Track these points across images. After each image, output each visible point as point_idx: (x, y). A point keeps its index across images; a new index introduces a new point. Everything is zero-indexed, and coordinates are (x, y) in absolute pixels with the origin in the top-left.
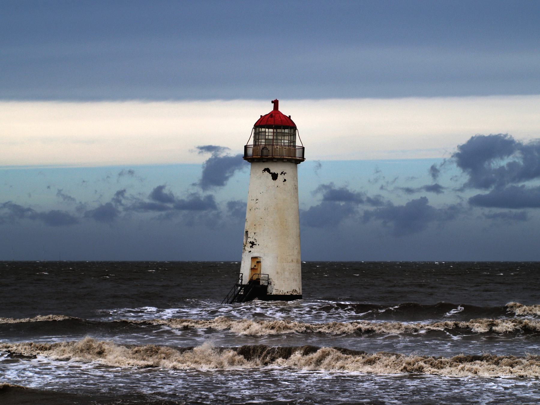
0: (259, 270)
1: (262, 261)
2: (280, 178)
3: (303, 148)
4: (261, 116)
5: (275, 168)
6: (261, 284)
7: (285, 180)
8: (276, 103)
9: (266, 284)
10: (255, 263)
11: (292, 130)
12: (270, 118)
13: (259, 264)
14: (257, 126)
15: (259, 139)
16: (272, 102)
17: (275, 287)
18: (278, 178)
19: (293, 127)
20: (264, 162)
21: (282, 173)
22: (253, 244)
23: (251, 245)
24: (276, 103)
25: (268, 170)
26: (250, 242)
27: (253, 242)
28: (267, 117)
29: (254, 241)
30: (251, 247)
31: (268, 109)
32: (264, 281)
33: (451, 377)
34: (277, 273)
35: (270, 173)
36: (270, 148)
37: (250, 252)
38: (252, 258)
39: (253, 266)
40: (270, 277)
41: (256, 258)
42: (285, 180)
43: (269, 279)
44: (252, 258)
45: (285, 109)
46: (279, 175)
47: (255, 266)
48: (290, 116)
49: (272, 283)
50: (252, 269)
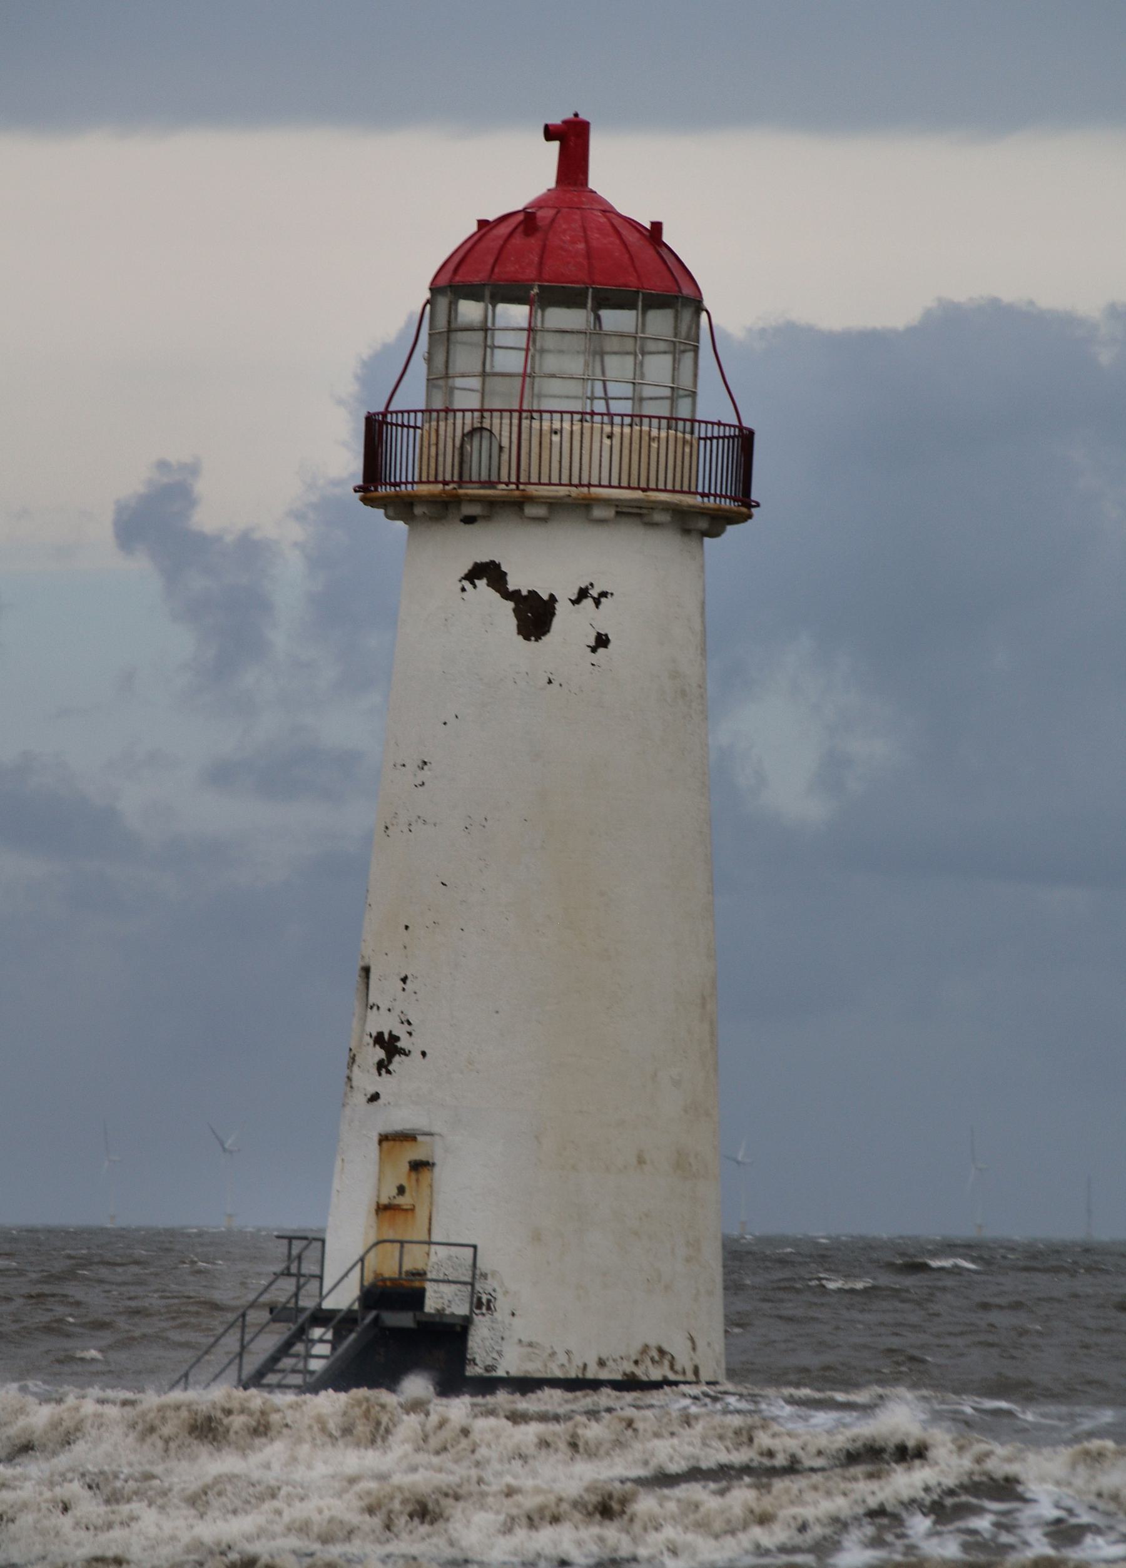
0: (422, 1214)
1: (438, 1158)
2: (571, 625)
3: (745, 440)
4: (482, 224)
5: (540, 560)
6: (431, 1305)
7: (602, 641)
8: (571, 139)
9: (461, 1309)
10: (400, 1173)
11: (687, 315)
12: (518, 240)
13: (425, 1174)
14: (458, 279)
15: (447, 376)
16: (550, 133)
17: (520, 1328)
18: (556, 623)
19: (697, 305)
20: (469, 520)
21: (583, 594)
22: (389, 1045)
23: (380, 1054)
24: (571, 139)
25: (488, 573)
26: (379, 1040)
27: (395, 1038)
28: (504, 230)
29: (400, 1031)
30: (382, 1066)
31: (527, 173)
32: (447, 1290)
33: (51, 1310)
34: (537, 1237)
35: (508, 595)
36: (503, 429)
37: (375, 1097)
38: (384, 1139)
39: (388, 1193)
40: (483, 1265)
41: (407, 1137)
42: (602, 641)
43: (476, 1273)
44: (384, 1139)
45: (624, 178)
46: (563, 608)
47: (401, 1190)
48: (657, 227)
49: (502, 1305)
50: (383, 1209)
